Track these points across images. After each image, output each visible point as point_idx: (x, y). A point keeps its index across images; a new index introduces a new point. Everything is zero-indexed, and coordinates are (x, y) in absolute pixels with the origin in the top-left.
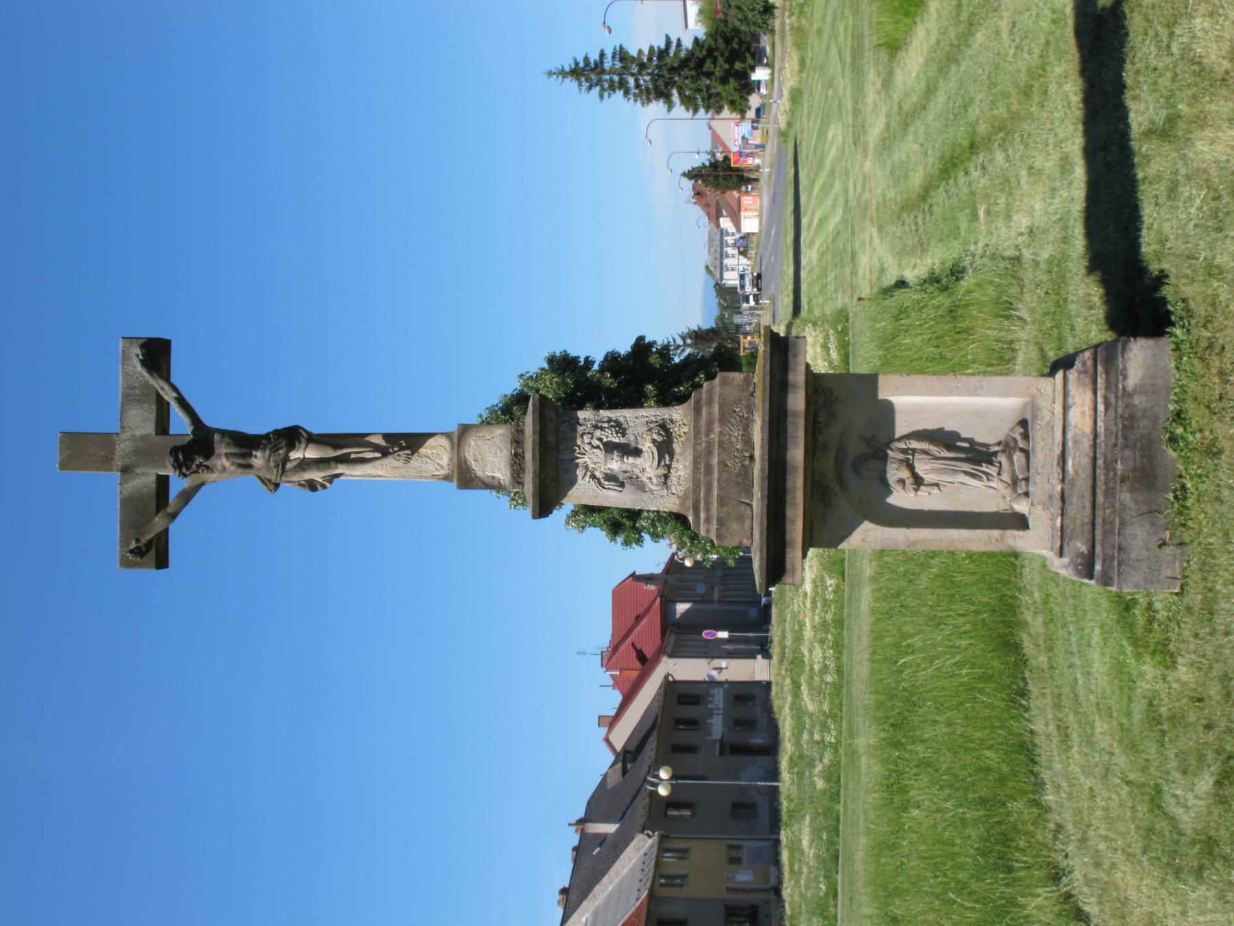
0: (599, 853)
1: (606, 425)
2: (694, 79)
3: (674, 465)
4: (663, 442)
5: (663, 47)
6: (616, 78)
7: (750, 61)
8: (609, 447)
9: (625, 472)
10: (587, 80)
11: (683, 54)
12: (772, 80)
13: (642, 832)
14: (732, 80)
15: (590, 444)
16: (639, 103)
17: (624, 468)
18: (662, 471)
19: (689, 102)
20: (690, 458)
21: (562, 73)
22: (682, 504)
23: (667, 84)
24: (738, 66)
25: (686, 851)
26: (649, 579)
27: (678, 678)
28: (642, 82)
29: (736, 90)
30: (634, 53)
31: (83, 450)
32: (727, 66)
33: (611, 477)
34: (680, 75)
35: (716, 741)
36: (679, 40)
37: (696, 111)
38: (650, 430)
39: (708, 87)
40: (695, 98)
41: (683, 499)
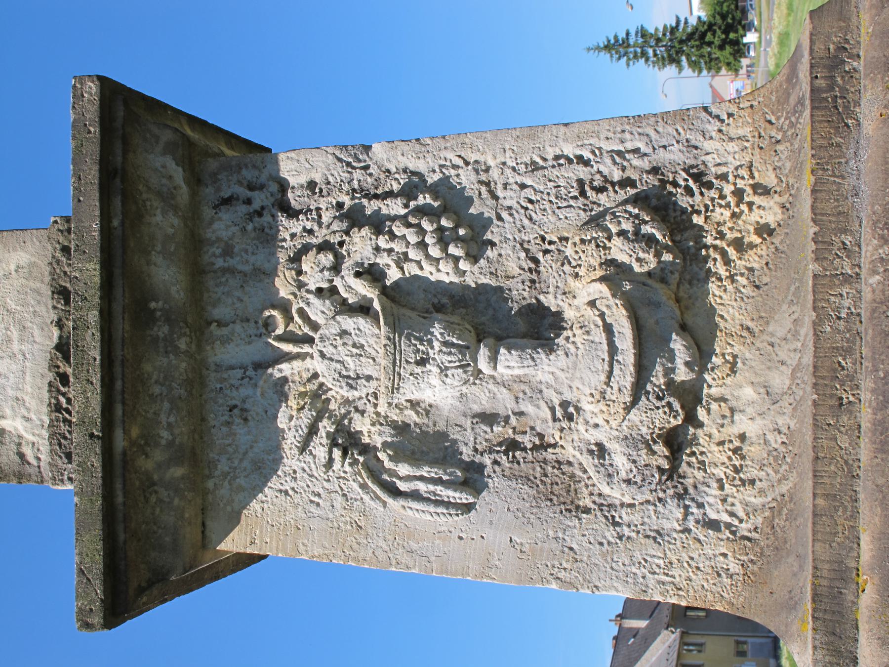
0: (633, 643)
1: (395, 207)
2: (699, 47)
3: (715, 384)
4: (660, 275)
5: (674, 25)
6: (639, 50)
7: (741, 32)
8: (407, 307)
9: (489, 418)
10: (616, 53)
11: (689, 30)
12: (760, 42)
13: (667, 628)
14: (727, 47)
15: (328, 293)
16: (656, 68)
17: (482, 398)
18: (653, 418)
19: (694, 65)
20: (799, 352)
21: (598, 48)
22: (752, 578)
23: (677, 53)
24: (732, 36)
25: (701, 645)
28: (658, 52)
29: (731, 54)
30: (652, 31)
32: (723, 36)
33: (425, 444)
34: (687, 45)
37: (700, 71)
38: (596, 221)
39: (710, 54)
40: (700, 62)
41: (762, 551)
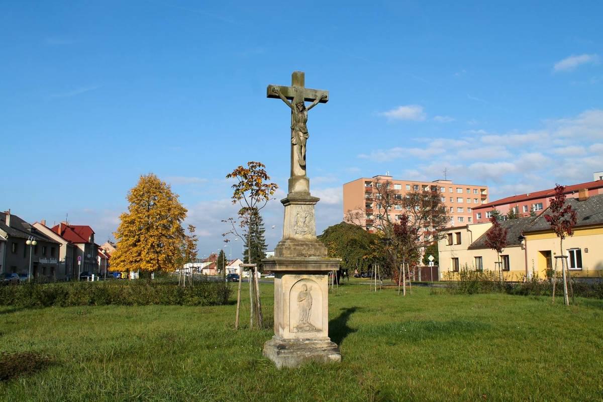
13: (7, 234)
26: (92, 239)
27: (61, 248)
31: (298, 78)
35: (39, 260)
36: (266, 249)
37: (244, 254)
